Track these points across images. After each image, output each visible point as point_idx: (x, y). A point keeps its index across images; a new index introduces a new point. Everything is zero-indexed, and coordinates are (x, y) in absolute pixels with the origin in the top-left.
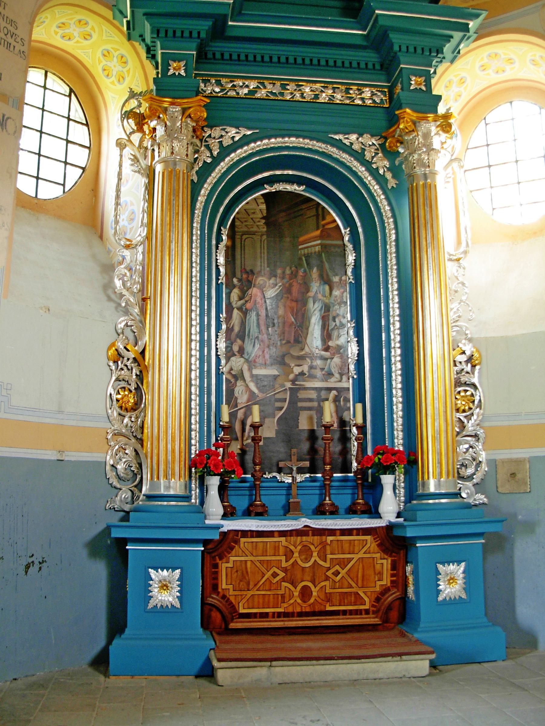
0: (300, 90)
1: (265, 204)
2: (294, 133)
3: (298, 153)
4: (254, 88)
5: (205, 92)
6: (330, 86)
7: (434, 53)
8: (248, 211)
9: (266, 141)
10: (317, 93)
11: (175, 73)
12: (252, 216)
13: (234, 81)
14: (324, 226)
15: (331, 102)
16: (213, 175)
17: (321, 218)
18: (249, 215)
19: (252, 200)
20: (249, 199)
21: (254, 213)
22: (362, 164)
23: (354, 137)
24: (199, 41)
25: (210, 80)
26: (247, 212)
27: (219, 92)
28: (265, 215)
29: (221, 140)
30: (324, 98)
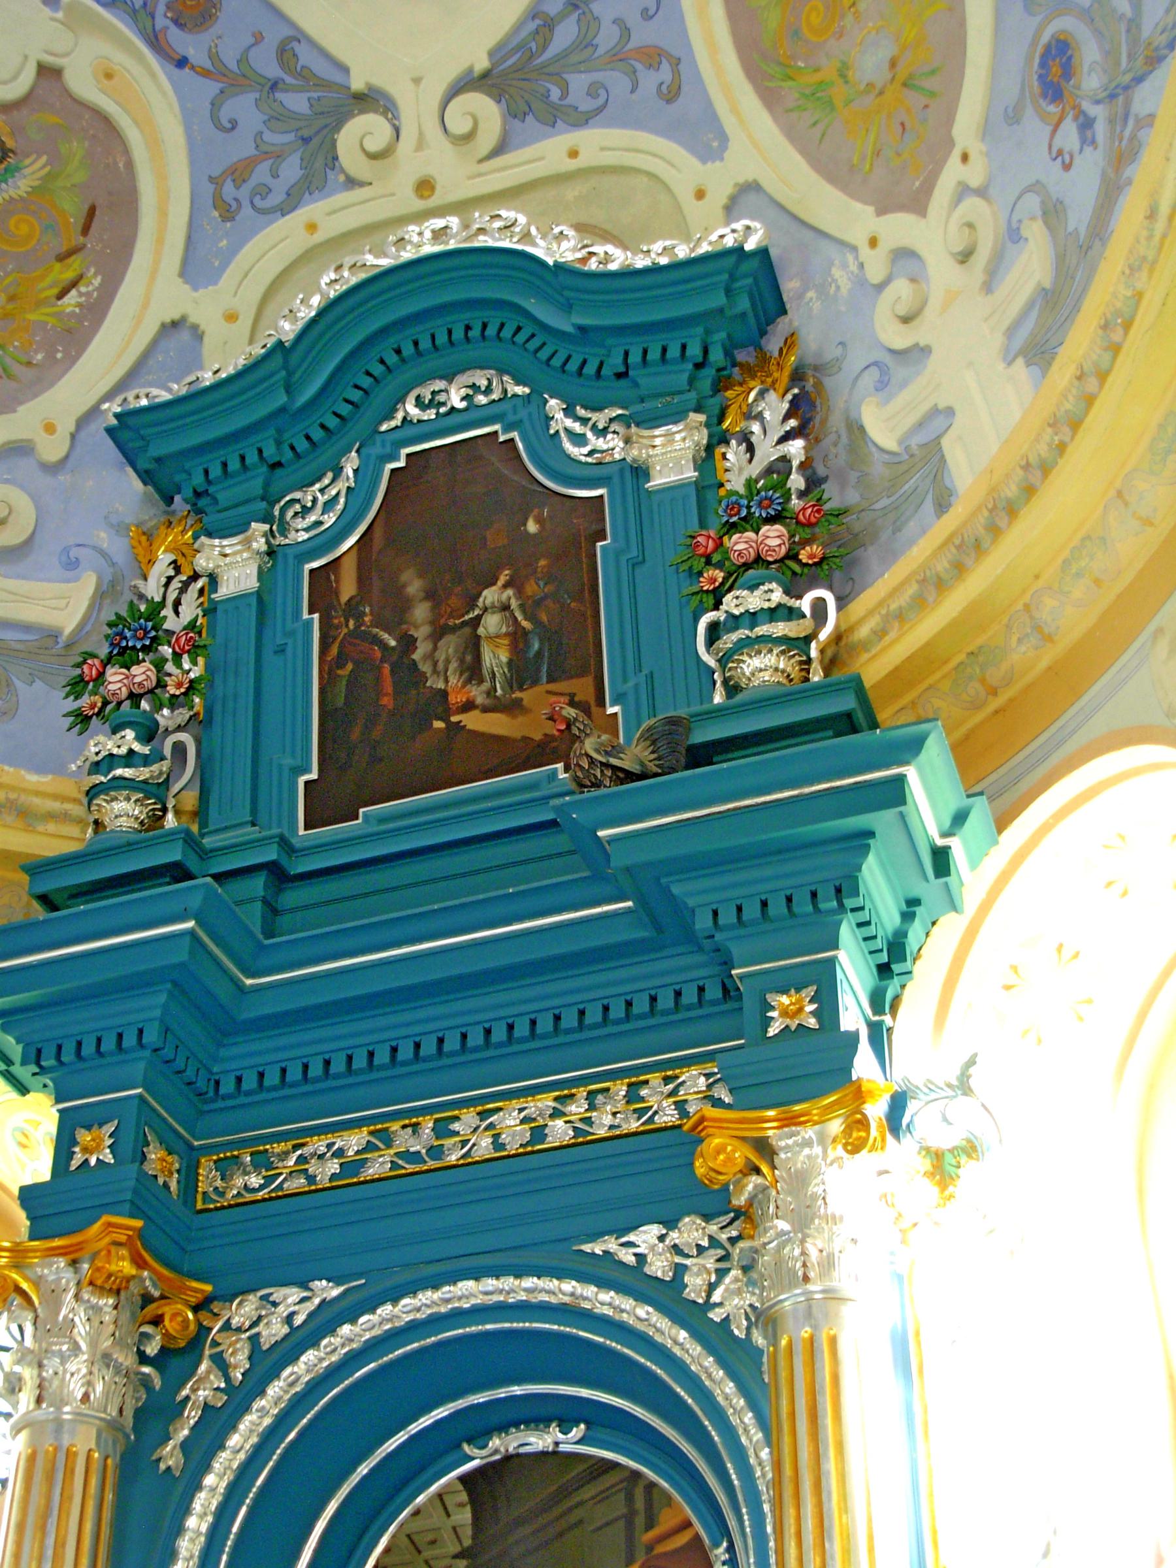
0: (491, 1126)
1: (468, 1508)
2: (465, 1263)
3: (473, 1329)
4: (358, 1153)
5: (222, 1194)
6: (582, 1092)
7: (830, 900)
8: (416, 1538)
9: (386, 1310)
10: (541, 1122)
11: (86, 1160)
12: (427, 1554)
13: (303, 1145)
14: (650, 1548)
15: (582, 1140)
16: (234, 1440)
17: (640, 1520)
18: (419, 1552)
19: (430, 1500)
20: (420, 1499)
21: (433, 1542)
22: (679, 1320)
23: (647, 1236)
24: (147, 1053)
25: (237, 1157)
26: (413, 1542)
27: (262, 1187)
28: (467, 1542)
29: (254, 1331)
30: (559, 1131)
